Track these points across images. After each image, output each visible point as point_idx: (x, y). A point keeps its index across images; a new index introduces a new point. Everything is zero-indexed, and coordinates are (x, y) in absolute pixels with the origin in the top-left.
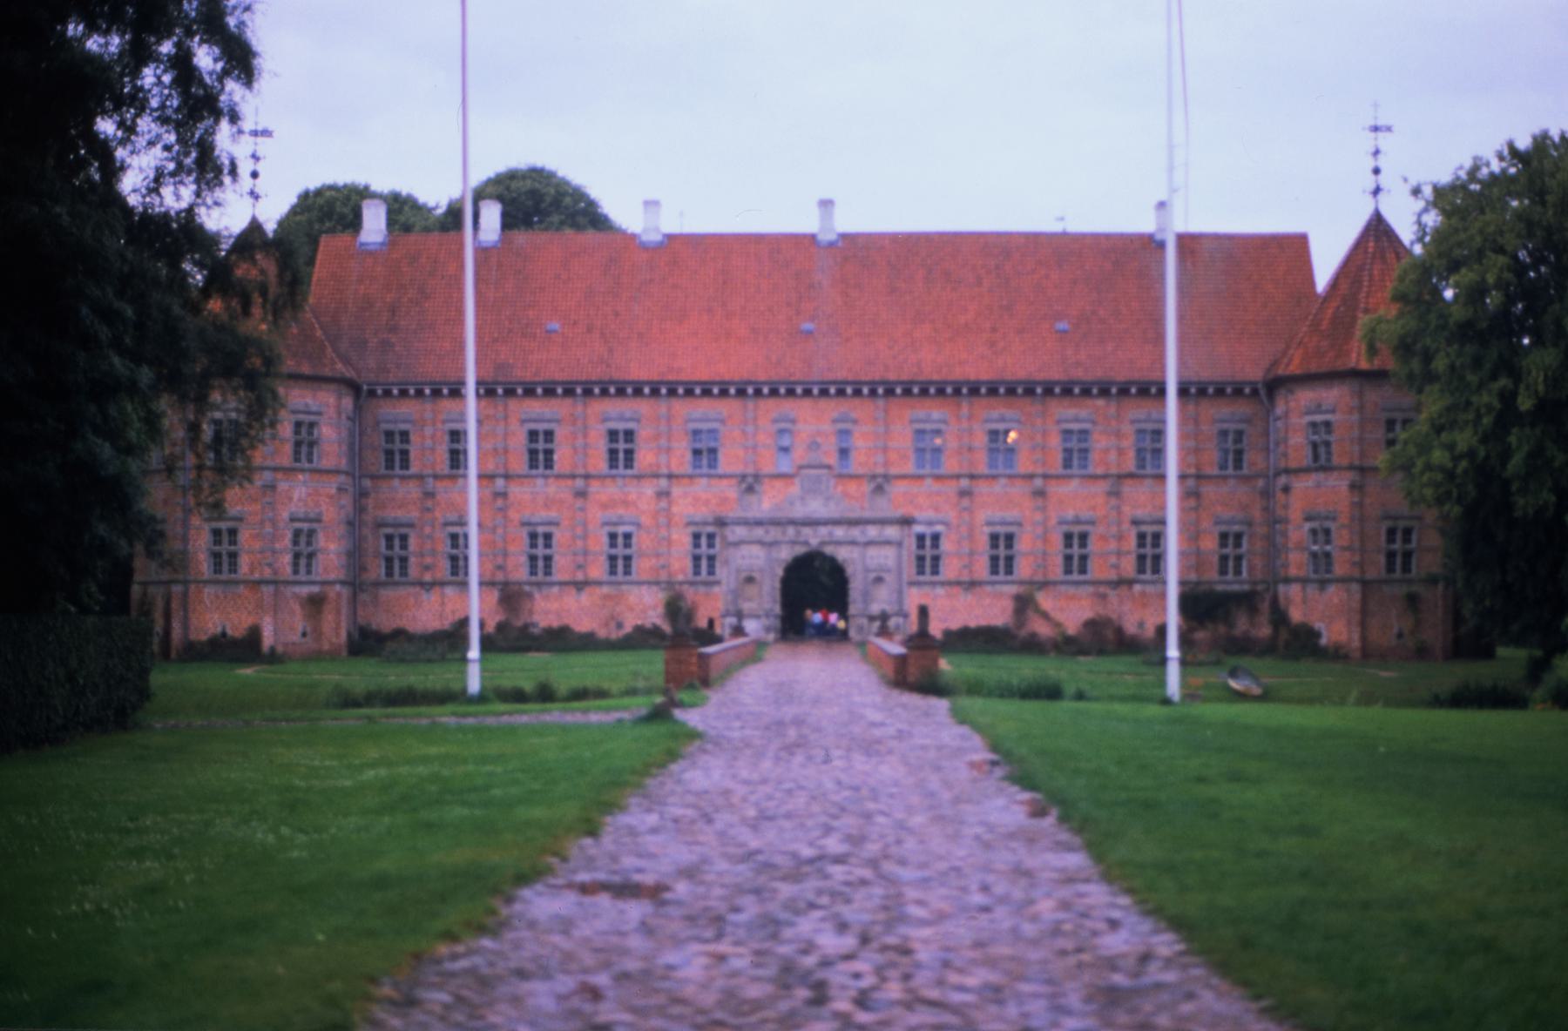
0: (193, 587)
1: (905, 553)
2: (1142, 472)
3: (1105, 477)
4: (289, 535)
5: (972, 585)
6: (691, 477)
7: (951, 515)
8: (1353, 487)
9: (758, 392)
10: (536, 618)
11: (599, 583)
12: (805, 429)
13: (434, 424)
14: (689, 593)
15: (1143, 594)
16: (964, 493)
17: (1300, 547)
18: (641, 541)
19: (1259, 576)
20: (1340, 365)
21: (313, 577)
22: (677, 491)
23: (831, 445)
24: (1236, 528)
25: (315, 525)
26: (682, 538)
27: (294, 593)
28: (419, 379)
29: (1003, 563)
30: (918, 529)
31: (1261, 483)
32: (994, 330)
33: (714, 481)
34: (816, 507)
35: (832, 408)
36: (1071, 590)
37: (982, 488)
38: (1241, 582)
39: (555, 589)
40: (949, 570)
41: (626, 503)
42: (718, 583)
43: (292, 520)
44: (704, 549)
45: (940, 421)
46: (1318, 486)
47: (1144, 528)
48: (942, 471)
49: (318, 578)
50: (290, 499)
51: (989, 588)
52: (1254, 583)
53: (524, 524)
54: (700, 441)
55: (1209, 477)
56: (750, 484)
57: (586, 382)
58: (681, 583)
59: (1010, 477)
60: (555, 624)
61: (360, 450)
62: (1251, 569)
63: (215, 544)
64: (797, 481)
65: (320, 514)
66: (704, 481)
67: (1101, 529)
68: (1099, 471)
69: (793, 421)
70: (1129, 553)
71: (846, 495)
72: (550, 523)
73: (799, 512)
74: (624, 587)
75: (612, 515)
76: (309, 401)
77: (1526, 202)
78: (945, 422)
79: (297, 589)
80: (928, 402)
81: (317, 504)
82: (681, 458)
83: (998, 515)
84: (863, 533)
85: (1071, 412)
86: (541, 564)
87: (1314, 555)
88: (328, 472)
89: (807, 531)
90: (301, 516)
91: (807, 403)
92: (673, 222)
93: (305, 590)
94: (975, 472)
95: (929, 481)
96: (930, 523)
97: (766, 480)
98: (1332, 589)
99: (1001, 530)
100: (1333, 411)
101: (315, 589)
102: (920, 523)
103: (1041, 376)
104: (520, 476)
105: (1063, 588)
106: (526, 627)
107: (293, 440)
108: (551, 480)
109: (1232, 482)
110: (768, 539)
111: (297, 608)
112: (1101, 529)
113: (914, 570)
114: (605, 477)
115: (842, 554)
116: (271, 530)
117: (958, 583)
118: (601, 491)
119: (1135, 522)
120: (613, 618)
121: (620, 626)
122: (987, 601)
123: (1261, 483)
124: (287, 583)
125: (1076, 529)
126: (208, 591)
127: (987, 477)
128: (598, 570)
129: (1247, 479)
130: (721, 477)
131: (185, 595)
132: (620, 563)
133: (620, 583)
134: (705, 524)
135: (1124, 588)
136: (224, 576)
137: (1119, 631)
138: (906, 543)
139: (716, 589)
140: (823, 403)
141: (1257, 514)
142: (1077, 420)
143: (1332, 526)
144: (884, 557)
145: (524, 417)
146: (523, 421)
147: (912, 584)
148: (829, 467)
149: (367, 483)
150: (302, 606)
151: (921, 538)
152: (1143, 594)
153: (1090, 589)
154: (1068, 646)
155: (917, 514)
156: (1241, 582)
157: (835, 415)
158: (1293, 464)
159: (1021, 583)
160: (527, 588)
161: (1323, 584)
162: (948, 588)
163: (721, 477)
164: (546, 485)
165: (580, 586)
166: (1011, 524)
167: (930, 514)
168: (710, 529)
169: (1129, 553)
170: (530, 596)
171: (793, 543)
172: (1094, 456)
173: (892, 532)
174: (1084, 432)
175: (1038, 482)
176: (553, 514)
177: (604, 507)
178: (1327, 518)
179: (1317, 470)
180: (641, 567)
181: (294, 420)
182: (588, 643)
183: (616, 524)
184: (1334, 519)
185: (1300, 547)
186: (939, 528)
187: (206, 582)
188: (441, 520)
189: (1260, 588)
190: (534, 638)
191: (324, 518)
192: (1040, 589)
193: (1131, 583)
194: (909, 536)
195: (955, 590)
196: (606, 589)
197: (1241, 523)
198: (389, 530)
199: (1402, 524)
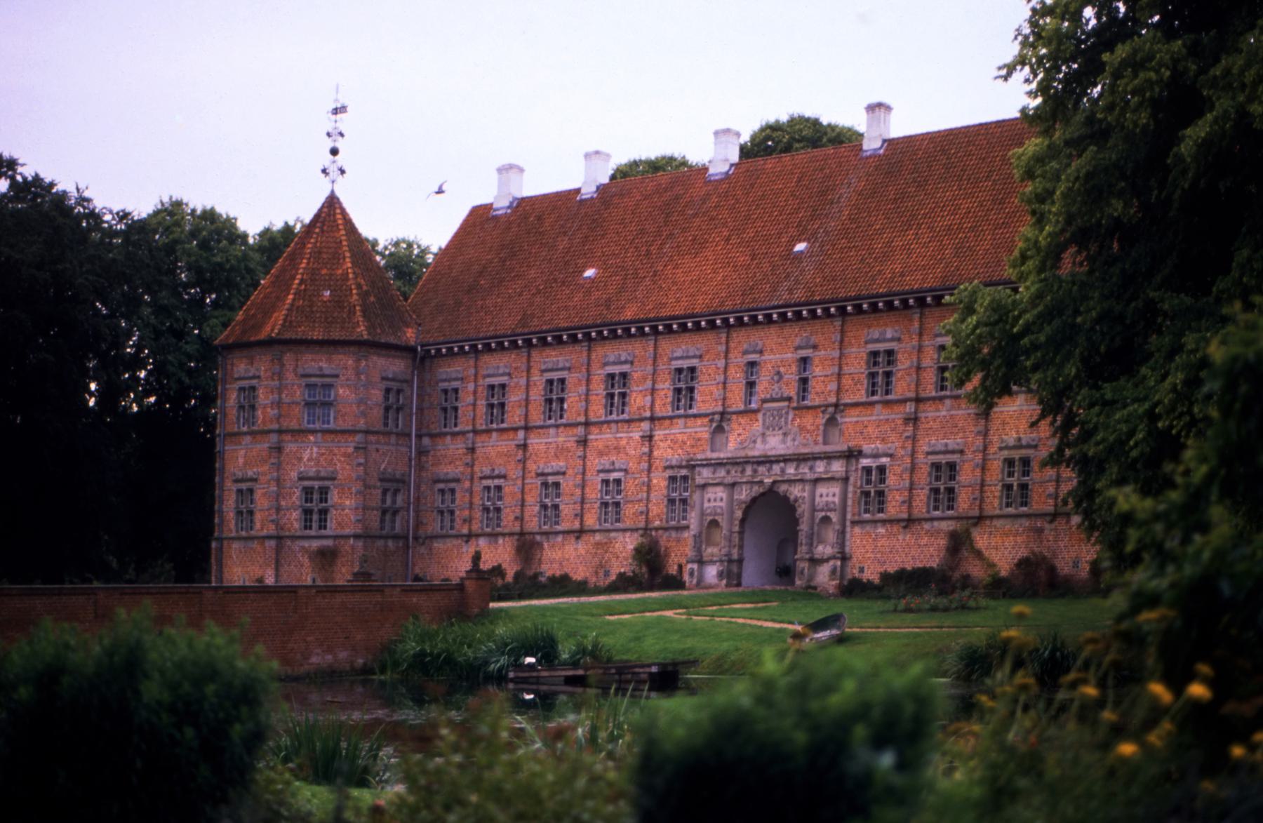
0: (225, 543)
1: (851, 489)
4: (298, 492)
5: (909, 522)
6: (671, 418)
7: (894, 444)
10: (544, 567)
11: (594, 531)
12: (770, 359)
13: (476, 381)
14: (664, 539)
18: (630, 486)
21: (328, 532)
22: (659, 434)
23: (792, 375)
25: (327, 483)
26: (659, 481)
27: (303, 547)
29: (944, 496)
30: (865, 462)
33: (690, 422)
34: (775, 444)
35: (797, 334)
39: (560, 538)
40: (894, 507)
42: (687, 527)
43: (301, 479)
45: (892, 340)
49: (506, 531)
50: (300, 459)
51: (927, 526)
53: (538, 475)
56: (720, 422)
58: (657, 529)
60: (558, 573)
61: (420, 409)
63: (306, 501)
64: (760, 416)
65: (335, 472)
66: (681, 422)
69: (761, 352)
71: (802, 428)
72: (557, 473)
73: (758, 450)
74: (613, 534)
75: (605, 462)
76: (324, 365)
77: (1150, 21)
79: (306, 544)
81: (331, 462)
83: (940, 444)
84: (811, 468)
86: (551, 511)
88: (343, 432)
90: (311, 474)
91: (773, 330)
92: (902, 125)
93: (315, 544)
97: (734, 417)
99: (943, 459)
101: (329, 543)
102: (866, 457)
104: (929, 399)
106: (536, 576)
107: (384, 405)
108: (561, 429)
110: (729, 480)
111: (306, 561)
114: (603, 423)
115: (796, 491)
116: (275, 488)
118: (599, 438)
120: (601, 566)
121: (607, 574)
124: (294, 538)
126: (236, 545)
131: (220, 549)
132: (611, 508)
133: (609, 531)
134: (680, 467)
137: (1052, 570)
139: (686, 534)
140: (788, 330)
144: (829, 494)
145: (543, 367)
146: (543, 371)
148: (789, 399)
149: (426, 441)
150: (310, 557)
151: (868, 470)
153: (1026, 523)
154: (1000, 588)
155: (867, 448)
157: (798, 341)
160: (538, 538)
164: (557, 435)
165: (580, 533)
166: (953, 452)
170: (540, 545)
171: (751, 483)
173: (838, 467)
176: (560, 464)
177: (601, 454)
180: (629, 510)
181: (384, 387)
182: (581, 588)
183: (609, 471)
186: (884, 460)
187: (233, 539)
188: (479, 475)
190: (544, 586)
191: (340, 476)
192: (975, 525)
196: (598, 537)
198: (441, 486)
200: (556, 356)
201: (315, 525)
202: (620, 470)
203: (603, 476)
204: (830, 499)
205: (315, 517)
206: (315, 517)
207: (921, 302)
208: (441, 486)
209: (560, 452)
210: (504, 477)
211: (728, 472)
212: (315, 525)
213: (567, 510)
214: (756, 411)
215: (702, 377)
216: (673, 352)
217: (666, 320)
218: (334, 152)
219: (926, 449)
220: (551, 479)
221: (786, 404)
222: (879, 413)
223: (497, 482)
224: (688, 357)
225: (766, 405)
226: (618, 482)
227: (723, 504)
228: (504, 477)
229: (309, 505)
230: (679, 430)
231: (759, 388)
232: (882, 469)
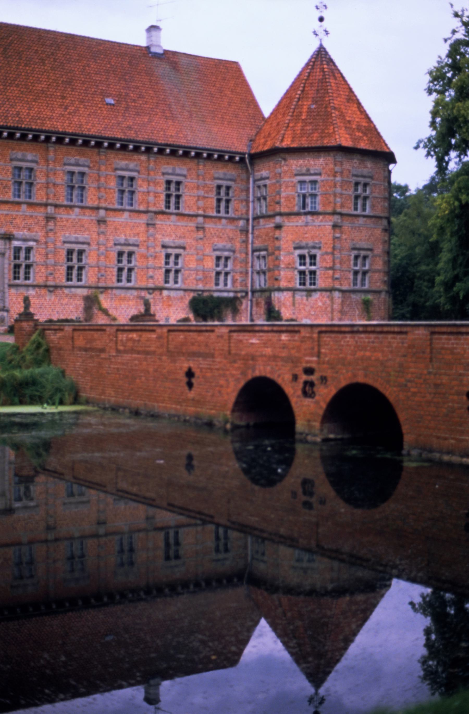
2: (167, 210)
3: (146, 212)
8: (335, 226)
15: (169, 297)
16: (101, 222)
17: (290, 266)
19: (239, 288)
20: (327, 142)
24: (226, 254)
30: (16, 243)
31: (241, 223)
32: (63, 98)
36: (122, 293)
37: (62, 214)
38: (228, 291)
44: (125, 263)
45: (32, 161)
46: (307, 225)
47: (170, 251)
48: (34, 200)
51: (66, 291)
52: (236, 292)
54: (304, 189)
55: (211, 217)
57: (24, 129)
59: (82, 208)
62: (234, 281)
67: (142, 250)
68: (142, 208)
70: (160, 268)
78: (36, 162)
85: (123, 163)
87: (302, 273)
94: (58, 202)
95: (24, 207)
96: (25, 240)
98: (316, 296)
100: (320, 174)
102: (18, 239)
103: (108, 134)
105: (117, 292)
109: (224, 221)
112: (142, 250)
113: (12, 276)
117: (46, 286)
119: (164, 247)
122: (65, 301)
123: (241, 223)
125: (127, 249)
127: (66, 206)
129: (232, 220)
135: (157, 293)
136: (20, 281)
138: (7, 255)
141: (238, 245)
142: (77, 165)
143: (318, 253)
147: (11, 286)
151: (18, 250)
152: (169, 297)
153: (135, 293)
155: (16, 233)
156: (228, 291)
158: (284, 210)
159: (89, 287)
161: (309, 292)
162: (37, 289)
166: (83, 243)
167: (26, 233)
169: (160, 268)
172: (137, 197)
174: (132, 179)
175: (102, 213)
178: (314, 247)
179: (306, 214)
184: (320, 248)
185: (290, 266)
186: (31, 244)
189: (239, 295)
193: (161, 289)
194: (10, 248)
195: (43, 291)
197: (229, 250)
199: (363, 253)
205: (308, 278)
206: (308, 278)
218: (321, 19)
219: (62, 239)
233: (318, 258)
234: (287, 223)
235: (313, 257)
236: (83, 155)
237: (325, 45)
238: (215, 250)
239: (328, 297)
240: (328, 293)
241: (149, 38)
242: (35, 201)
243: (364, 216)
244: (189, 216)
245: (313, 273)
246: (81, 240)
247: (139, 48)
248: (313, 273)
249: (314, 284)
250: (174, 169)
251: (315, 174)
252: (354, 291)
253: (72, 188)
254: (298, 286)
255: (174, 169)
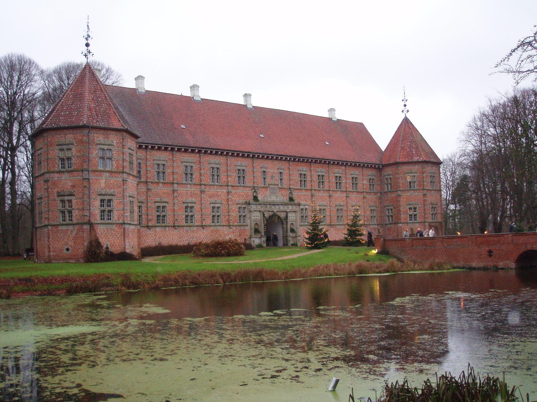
9: (233, 154)
17: (406, 212)
22: (428, 194)
23: (277, 177)
28: (186, 145)
30: (302, 207)
33: (244, 188)
34: (273, 199)
40: (169, 220)
41: (218, 196)
57: (228, 150)
64: (268, 189)
66: (241, 188)
75: (212, 200)
78: (307, 171)
80: (303, 164)
82: (233, 179)
83: (321, 203)
87: (411, 215)
89: (273, 207)
91: (270, 161)
95: (339, 193)
96: (305, 205)
100: (416, 173)
102: (302, 205)
105: (338, 227)
109: (355, 193)
128: (208, 222)
130: (246, 187)
143: (417, 207)
148: (277, 185)
151: (302, 209)
155: (302, 203)
163: (246, 187)
168: (244, 206)
176: (194, 200)
177: (210, 197)
185: (406, 212)
197: (375, 207)
200: (188, 157)
201: (413, 219)
202: (219, 203)
203: (212, 205)
204: (293, 218)
205: (413, 217)
206: (413, 217)
207: (329, 163)
208: (387, 208)
209: (192, 195)
210: (167, 202)
211: (262, 207)
212: (413, 219)
213: (197, 217)
214: (267, 188)
215: (247, 174)
216: (237, 163)
217: (140, 143)
218: (405, 106)
220: (190, 205)
221: (276, 186)
222: (304, 193)
223: (163, 204)
224: (242, 166)
225: (270, 186)
226: (218, 208)
227: (259, 218)
228: (167, 202)
229: (415, 213)
230: (241, 191)
231: (267, 180)
232: (306, 209)
233: (417, 209)
234: (403, 194)
235: (415, 208)
236: (323, 168)
237: (407, 116)
238: (370, 207)
239: (423, 225)
240: (423, 224)
241: (246, 100)
242: (307, 188)
243: (434, 190)
244: (360, 192)
245: (415, 215)
246: (324, 204)
247: (181, 98)
248: (415, 215)
249: (416, 220)
250: (354, 172)
251: (414, 173)
252: (239, 226)
253: (186, 174)
254: (409, 221)
255: (354, 172)
